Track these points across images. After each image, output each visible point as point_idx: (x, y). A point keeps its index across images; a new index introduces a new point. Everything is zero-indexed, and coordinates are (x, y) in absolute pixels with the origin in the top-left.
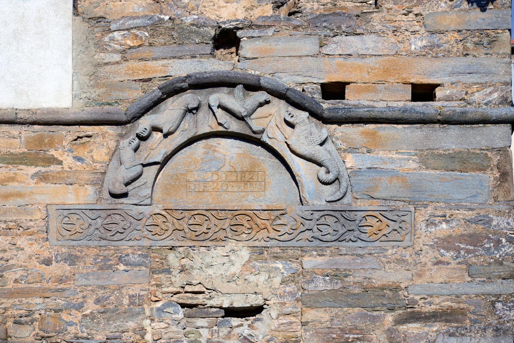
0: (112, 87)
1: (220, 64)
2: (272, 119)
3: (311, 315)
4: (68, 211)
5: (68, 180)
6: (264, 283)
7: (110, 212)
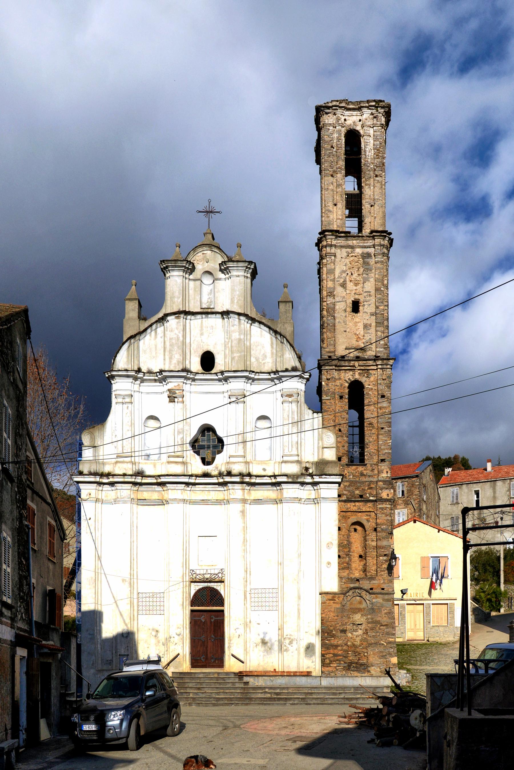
0: (343, 588)
1: (357, 585)
2: (364, 593)
3: (369, 625)
4: (337, 608)
5: (337, 603)
6: (363, 620)
7: (342, 609)
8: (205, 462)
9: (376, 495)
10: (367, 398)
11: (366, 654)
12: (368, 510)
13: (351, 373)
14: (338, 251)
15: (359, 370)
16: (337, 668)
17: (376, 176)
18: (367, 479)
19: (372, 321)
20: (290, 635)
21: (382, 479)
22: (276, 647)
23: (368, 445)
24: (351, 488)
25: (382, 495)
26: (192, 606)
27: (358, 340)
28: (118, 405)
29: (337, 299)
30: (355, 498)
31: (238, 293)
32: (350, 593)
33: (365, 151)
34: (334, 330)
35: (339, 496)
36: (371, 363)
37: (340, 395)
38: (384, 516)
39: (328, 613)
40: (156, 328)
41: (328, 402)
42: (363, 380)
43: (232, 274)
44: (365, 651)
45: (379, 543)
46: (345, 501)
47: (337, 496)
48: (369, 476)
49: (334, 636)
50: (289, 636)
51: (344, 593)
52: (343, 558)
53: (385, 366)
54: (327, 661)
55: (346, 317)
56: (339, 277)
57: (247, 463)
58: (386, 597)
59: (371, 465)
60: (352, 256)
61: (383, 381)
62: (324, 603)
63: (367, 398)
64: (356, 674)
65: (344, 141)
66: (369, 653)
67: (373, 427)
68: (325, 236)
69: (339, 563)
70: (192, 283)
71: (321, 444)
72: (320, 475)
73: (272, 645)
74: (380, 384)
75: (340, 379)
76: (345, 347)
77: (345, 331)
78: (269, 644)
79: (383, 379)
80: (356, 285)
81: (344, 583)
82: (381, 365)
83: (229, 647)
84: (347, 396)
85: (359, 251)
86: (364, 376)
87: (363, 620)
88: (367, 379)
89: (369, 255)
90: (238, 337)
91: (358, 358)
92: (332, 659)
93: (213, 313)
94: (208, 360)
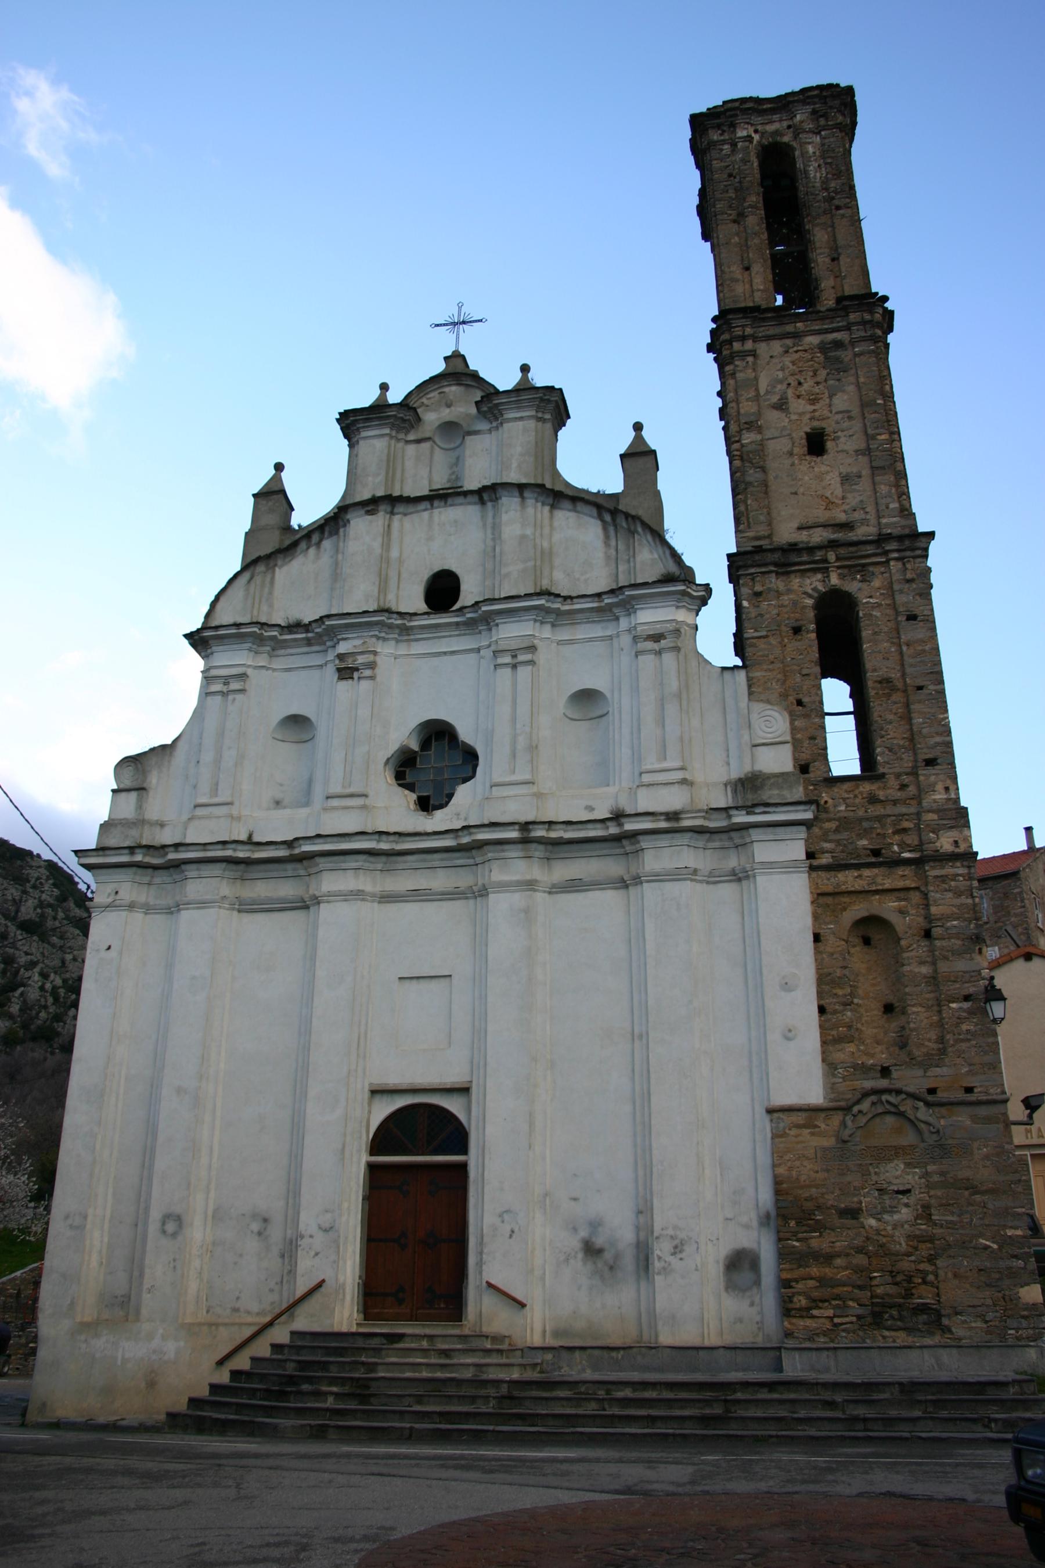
1: (883, 1083)
4: (825, 1149)
6: (912, 1178)
8: (425, 805)
9: (919, 847)
10: (868, 625)
11: (931, 1278)
12: (900, 884)
13: (819, 576)
14: (762, 348)
15: (838, 567)
16: (836, 1320)
17: (838, 208)
18: (889, 810)
19: (862, 465)
20: (675, 1227)
21: (935, 806)
22: (628, 1262)
23: (882, 729)
24: (844, 835)
25: (938, 844)
26: (372, 1154)
27: (831, 506)
28: (209, 698)
29: (768, 434)
30: (859, 856)
31: (519, 449)
32: (865, 1106)
33: (806, 172)
34: (766, 493)
35: (810, 855)
36: (870, 549)
37: (795, 625)
38: (950, 895)
39: (797, 1163)
40: (321, 541)
41: (762, 644)
42: (852, 587)
43: (506, 416)
44: (925, 1266)
45: (943, 967)
46: (828, 868)
47: (804, 857)
48: (895, 802)
49: (820, 1227)
50: (670, 1232)
51: (839, 1107)
52: (835, 1012)
53: (908, 553)
54: (802, 1301)
55: (793, 465)
56: (767, 392)
57: (539, 795)
58: (983, 1111)
59: (898, 776)
60: (796, 352)
61: (907, 586)
62: (781, 1136)
63: (868, 625)
64: (902, 1338)
65: (756, 164)
66: (941, 1273)
67: (894, 689)
68: (728, 323)
69: (821, 1026)
70: (411, 449)
71: (746, 737)
72: (749, 809)
73: (617, 1257)
74: (901, 591)
75: (789, 591)
76: (796, 525)
77: (796, 493)
78: (608, 1256)
79: (908, 581)
80: (813, 401)
81: (844, 1078)
82: (898, 551)
83: (480, 1263)
84: (813, 626)
85: (813, 340)
86: (855, 579)
87: (912, 1178)
88: (864, 585)
89: (838, 344)
90: (518, 532)
91: (833, 544)
92: (815, 1294)
93: (458, 494)
94: (442, 590)
